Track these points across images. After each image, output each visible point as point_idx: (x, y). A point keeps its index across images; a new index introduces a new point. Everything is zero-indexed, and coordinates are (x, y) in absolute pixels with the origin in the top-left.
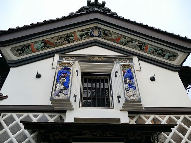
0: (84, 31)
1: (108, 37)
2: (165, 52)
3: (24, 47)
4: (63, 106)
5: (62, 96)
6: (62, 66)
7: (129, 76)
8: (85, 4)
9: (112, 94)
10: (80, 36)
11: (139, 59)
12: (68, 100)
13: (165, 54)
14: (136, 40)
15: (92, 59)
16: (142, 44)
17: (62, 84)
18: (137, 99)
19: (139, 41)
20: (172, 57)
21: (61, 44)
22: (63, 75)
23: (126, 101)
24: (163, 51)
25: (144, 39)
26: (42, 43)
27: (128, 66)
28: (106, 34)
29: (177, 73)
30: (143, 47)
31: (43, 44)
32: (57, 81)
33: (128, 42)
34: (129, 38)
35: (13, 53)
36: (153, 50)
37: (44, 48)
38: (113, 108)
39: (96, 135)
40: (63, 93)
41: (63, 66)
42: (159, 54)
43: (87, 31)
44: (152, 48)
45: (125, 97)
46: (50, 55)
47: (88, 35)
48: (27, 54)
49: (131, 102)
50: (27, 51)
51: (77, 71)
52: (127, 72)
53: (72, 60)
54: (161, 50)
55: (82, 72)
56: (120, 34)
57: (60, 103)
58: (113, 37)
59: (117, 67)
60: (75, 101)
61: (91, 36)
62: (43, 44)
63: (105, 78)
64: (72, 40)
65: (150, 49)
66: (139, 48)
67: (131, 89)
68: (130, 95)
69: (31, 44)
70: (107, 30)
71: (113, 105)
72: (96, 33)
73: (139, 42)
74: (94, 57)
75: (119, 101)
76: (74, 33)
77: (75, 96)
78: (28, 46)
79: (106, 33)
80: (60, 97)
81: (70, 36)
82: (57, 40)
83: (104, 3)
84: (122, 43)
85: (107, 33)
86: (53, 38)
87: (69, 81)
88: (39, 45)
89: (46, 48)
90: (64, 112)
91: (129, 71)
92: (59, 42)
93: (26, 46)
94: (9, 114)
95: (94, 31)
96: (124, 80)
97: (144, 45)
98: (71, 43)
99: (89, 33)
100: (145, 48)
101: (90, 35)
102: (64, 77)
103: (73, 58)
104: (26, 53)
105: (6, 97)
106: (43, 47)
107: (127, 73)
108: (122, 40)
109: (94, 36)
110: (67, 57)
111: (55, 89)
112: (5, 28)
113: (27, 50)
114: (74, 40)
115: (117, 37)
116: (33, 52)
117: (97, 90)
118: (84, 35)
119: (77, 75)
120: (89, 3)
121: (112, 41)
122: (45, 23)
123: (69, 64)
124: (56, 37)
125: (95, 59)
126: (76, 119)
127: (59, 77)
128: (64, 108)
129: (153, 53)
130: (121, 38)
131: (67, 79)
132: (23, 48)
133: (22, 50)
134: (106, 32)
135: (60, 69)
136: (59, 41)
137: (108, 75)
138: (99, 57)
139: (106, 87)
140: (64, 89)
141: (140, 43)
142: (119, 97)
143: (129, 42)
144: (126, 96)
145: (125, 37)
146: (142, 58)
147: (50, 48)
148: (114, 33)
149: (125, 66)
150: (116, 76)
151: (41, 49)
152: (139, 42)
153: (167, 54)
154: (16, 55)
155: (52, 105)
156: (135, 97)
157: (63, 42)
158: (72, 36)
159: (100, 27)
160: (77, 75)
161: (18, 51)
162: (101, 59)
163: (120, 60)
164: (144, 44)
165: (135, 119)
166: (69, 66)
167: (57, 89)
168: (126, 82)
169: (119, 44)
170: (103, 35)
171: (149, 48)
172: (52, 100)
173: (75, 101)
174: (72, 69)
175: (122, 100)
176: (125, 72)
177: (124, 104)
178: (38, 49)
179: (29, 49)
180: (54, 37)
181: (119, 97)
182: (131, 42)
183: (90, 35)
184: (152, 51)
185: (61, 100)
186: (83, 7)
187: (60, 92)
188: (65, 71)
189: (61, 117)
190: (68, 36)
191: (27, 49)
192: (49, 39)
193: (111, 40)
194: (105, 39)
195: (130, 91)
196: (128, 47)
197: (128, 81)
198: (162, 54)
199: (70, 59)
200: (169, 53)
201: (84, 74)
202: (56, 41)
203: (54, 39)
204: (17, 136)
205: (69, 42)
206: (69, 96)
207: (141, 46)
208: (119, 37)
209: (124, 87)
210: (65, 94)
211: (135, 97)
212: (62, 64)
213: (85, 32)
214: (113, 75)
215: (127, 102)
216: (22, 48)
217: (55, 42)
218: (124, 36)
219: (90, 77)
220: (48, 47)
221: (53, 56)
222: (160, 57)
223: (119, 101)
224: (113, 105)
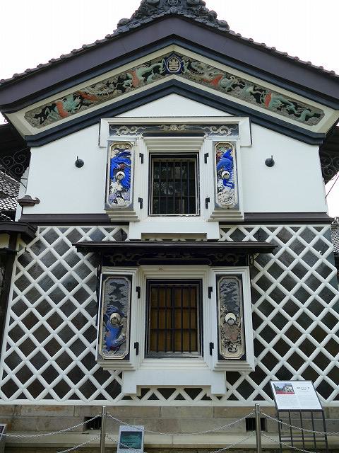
0: (150, 65)
1: (197, 76)
3: (45, 109)
4: (127, 217)
5: (121, 202)
6: (116, 149)
7: (226, 163)
10: (143, 76)
11: (251, 122)
12: (131, 207)
15: (165, 129)
18: (234, 204)
19: (255, 86)
23: (217, 207)
25: (146, 324)
27: (226, 144)
31: (78, 100)
32: (111, 178)
33: (234, 86)
34: (236, 77)
35: (29, 121)
36: (280, 103)
38: (199, 216)
39: (171, 257)
41: (118, 149)
42: (291, 112)
43: (155, 65)
44: (278, 99)
46: (92, 120)
47: (158, 72)
48: (53, 122)
49: (223, 209)
51: (141, 156)
55: (150, 153)
58: (206, 76)
59: (206, 146)
60: (141, 207)
61: (163, 74)
62: (78, 100)
63: (189, 162)
64: (129, 86)
66: (255, 100)
67: (227, 189)
68: (223, 199)
70: (195, 61)
73: (255, 86)
74: (169, 125)
75: (207, 207)
76: (132, 71)
77: (140, 200)
79: (194, 67)
82: (101, 89)
84: (223, 89)
85: (196, 68)
86: (93, 87)
88: (71, 103)
90: (127, 224)
91: (228, 156)
94: (48, 228)
98: (128, 91)
99: (159, 67)
101: (161, 72)
103: (132, 128)
105: (38, 201)
106: (77, 106)
108: (224, 81)
110: (122, 128)
112: (7, 75)
114: (132, 87)
117: (174, 184)
118: (150, 73)
119: (142, 162)
122: (77, 55)
123: (127, 144)
124: (100, 82)
126: (143, 235)
127: (114, 171)
128: (126, 220)
133: (42, 116)
135: (113, 154)
136: (105, 91)
137: (195, 156)
140: (124, 191)
142: (208, 200)
144: (217, 202)
145: (228, 76)
146: (257, 119)
150: (206, 162)
152: (255, 86)
153: (305, 112)
154: (35, 126)
156: (232, 202)
158: (128, 78)
160: (142, 162)
161: (36, 117)
164: (265, 91)
165: (230, 232)
167: (113, 190)
172: (107, 207)
173: (141, 207)
181: (208, 200)
183: (161, 72)
185: (120, 209)
189: (122, 231)
190: (121, 80)
193: (202, 81)
194: (190, 79)
195: (224, 191)
196: (234, 96)
198: (296, 112)
199: (128, 130)
200: (309, 110)
201: (153, 156)
203: (96, 88)
205: (124, 91)
207: (258, 96)
208: (217, 75)
209: (215, 185)
211: (232, 202)
216: (44, 110)
220: (88, 105)
221: (99, 122)
222: (292, 118)
223: (207, 207)
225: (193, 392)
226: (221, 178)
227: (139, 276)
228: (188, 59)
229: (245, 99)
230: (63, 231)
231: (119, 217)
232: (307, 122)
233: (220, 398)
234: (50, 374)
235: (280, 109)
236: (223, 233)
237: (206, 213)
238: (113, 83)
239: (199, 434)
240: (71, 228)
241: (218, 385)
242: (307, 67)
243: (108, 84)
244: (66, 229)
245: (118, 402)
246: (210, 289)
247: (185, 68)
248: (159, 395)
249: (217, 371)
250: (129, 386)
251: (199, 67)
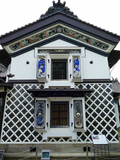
1: (67, 34)
3: (16, 44)
4: (43, 81)
7: (77, 63)
8: (52, 5)
10: (49, 33)
11: (85, 49)
12: (45, 78)
18: (79, 77)
19: (86, 37)
20: (106, 47)
21: (38, 40)
23: (74, 77)
24: (100, 43)
26: (26, 41)
27: (77, 57)
28: (65, 31)
29: (107, 58)
31: (27, 42)
32: (39, 68)
33: (79, 37)
34: (80, 34)
35: (11, 49)
36: (95, 42)
39: (59, 94)
41: (41, 58)
42: (98, 46)
43: (53, 30)
45: (73, 76)
47: (54, 32)
48: (19, 49)
51: (49, 60)
53: (45, 52)
54: (99, 43)
55: (51, 59)
57: (41, 80)
58: (70, 33)
59: (70, 57)
62: (27, 42)
63: (64, 62)
66: (86, 41)
67: (77, 71)
70: (66, 28)
74: (58, 50)
75: (70, 77)
76: (45, 32)
77: (48, 75)
78: (19, 44)
80: (41, 76)
82: (35, 38)
83: (65, 3)
84: (76, 38)
85: (66, 31)
86: (32, 37)
88: (24, 43)
90: (44, 83)
91: (77, 60)
92: (37, 39)
93: (17, 44)
95: (58, 29)
98: (44, 39)
99: (54, 30)
100: (89, 41)
102: (42, 65)
105: (14, 76)
107: (76, 62)
108: (76, 35)
111: (38, 72)
116: (22, 47)
118: (51, 32)
119: (49, 62)
121: (69, 36)
123: (44, 56)
127: (39, 66)
133: (15, 47)
135: (39, 60)
136: (36, 38)
140: (43, 72)
141: (87, 38)
142: (71, 75)
143: (80, 37)
144: (74, 76)
145: (77, 33)
146: (87, 48)
150: (70, 62)
153: (103, 46)
154: (13, 50)
155: (37, 79)
156: (79, 76)
157: (39, 39)
158: (44, 34)
160: (49, 62)
161: (13, 47)
163: (73, 52)
164: (90, 39)
165: (78, 86)
167: (39, 72)
168: (75, 67)
170: (64, 32)
172: (37, 78)
174: (45, 59)
180: (33, 36)
181: (71, 75)
183: (55, 32)
184: (94, 44)
185: (41, 78)
186: (50, 8)
188: (42, 61)
192: (30, 38)
193: (69, 35)
195: (76, 72)
199: (44, 52)
200: (104, 45)
201: (53, 60)
202: (35, 39)
204: (24, 94)
205: (43, 38)
206: (45, 76)
207: (87, 40)
213: (52, 30)
216: (16, 45)
220: (30, 43)
221: (34, 49)
223: (70, 77)
225: (66, 139)
227: (47, 101)
229: (83, 41)
230: (23, 85)
233: (75, 141)
234: (18, 133)
236: (76, 86)
237: (70, 79)
240: (25, 85)
241: (74, 136)
243: (37, 36)
244: (24, 85)
245: (41, 142)
246: (72, 105)
247: (63, 31)
248: (63, 140)
249: (74, 132)
250: (45, 137)
251: (68, 31)
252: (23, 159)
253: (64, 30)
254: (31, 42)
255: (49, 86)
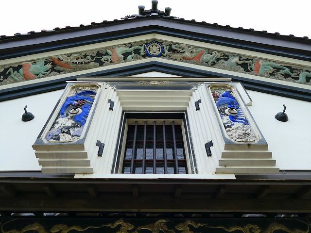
0: (131, 47)
2: (296, 70)
3: (9, 68)
6: (78, 89)
9: (192, 148)
10: (123, 54)
12: (80, 145)
13: (298, 75)
14: (234, 55)
16: (248, 60)
17: (72, 118)
19: (240, 56)
22: (76, 102)
23: (229, 145)
26: (46, 63)
30: (250, 65)
31: (49, 66)
33: (218, 60)
34: (219, 52)
36: (272, 69)
37: (50, 73)
40: (70, 134)
42: (286, 76)
44: (268, 65)
47: (139, 53)
48: (13, 82)
49: (239, 146)
50: (15, 77)
52: (223, 96)
54: (288, 67)
55: (123, 111)
56: (201, 47)
58: (187, 54)
61: (144, 56)
62: (49, 66)
64: (108, 61)
65: (265, 68)
68: (235, 135)
69: (23, 63)
70: (175, 43)
71: (194, 168)
72: (155, 49)
73: (240, 57)
75: (209, 154)
76: (112, 48)
77: (101, 146)
78: (18, 68)
80: (61, 140)
81: (104, 53)
82: (77, 59)
83: (168, 11)
84: (206, 63)
86: (69, 55)
87: (89, 112)
88: (40, 67)
89: (54, 72)
92: (82, 63)
95: (151, 47)
96: (218, 109)
97: (251, 61)
98: (106, 65)
100: (253, 66)
101: (142, 54)
104: (12, 80)
106: (47, 71)
108: (206, 57)
109: (151, 56)
111: (52, 127)
113: (15, 75)
114: (111, 62)
115: (196, 52)
116: (27, 79)
118: (130, 53)
119: (111, 109)
120: (141, 9)
121: (186, 62)
124: (77, 53)
125: (152, 83)
129: (272, 75)
130: (202, 54)
131: (86, 110)
132: (6, 72)
134: (174, 47)
136: (81, 61)
138: (159, 81)
139: (180, 157)
140: (74, 126)
141: (241, 59)
142: (208, 146)
143: (220, 59)
144: (227, 137)
145: (210, 51)
146: (249, 85)
147: (62, 73)
148: (189, 46)
149: (217, 87)
150: (198, 109)
151: (44, 74)
152: (240, 57)
158: (107, 54)
159: (161, 40)
162: (164, 83)
166: (94, 90)
167: (57, 126)
168: (224, 112)
169: (201, 64)
171: (261, 67)
175: (218, 149)
176: (218, 97)
177: (224, 155)
178: (37, 75)
179: (18, 72)
180: (71, 54)
181: (208, 146)
182: (224, 59)
183: (142, 54)
184: (270, 72)
187: (63, 132)
190: (99, 54)
191: (16, 72)
193: (184, 59)
195: (234, 127)
197: (227, 111)
198: (292, 75)
200: (307, 71)
202: (75, 61)
203: (71, 57)
205: (102, 64)
206: (81, 137)
207: (245, 66)
208: (199, 52)
209: (219, 121)
210: (73, 136)
212: (80, 86)
214: (191, 111)
215: (232, 149)
216: (6, 70)
217: (73, 62)
218: (209, 49)
219: (141, 121)
220: (59, 72)
223: (209, 154)
224: (194, 168)
226: (225, 114)
228: (168, 44)
229: (231, 69)
231: (58, 163)
232: (309, 83)
235: (274, 75)
238: (91, 56)
239: (134, 16)
242: (291, 38)
243: (85, 56)
247: (166, 51)
251: (180, 48)
252: (235, 232)
253: (171, 49)
254: (61, 69)
255: (96, 146)
